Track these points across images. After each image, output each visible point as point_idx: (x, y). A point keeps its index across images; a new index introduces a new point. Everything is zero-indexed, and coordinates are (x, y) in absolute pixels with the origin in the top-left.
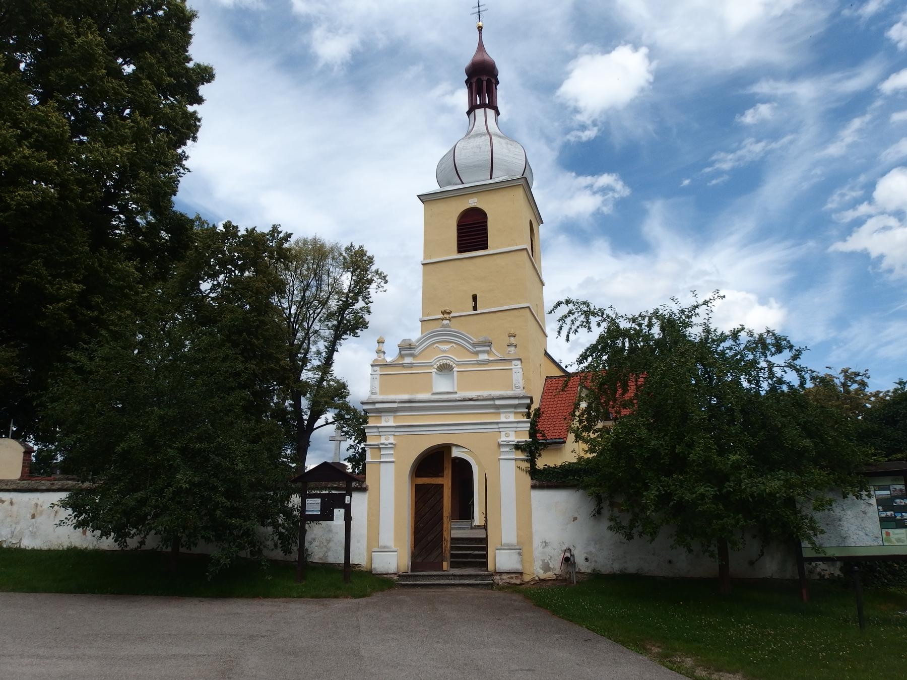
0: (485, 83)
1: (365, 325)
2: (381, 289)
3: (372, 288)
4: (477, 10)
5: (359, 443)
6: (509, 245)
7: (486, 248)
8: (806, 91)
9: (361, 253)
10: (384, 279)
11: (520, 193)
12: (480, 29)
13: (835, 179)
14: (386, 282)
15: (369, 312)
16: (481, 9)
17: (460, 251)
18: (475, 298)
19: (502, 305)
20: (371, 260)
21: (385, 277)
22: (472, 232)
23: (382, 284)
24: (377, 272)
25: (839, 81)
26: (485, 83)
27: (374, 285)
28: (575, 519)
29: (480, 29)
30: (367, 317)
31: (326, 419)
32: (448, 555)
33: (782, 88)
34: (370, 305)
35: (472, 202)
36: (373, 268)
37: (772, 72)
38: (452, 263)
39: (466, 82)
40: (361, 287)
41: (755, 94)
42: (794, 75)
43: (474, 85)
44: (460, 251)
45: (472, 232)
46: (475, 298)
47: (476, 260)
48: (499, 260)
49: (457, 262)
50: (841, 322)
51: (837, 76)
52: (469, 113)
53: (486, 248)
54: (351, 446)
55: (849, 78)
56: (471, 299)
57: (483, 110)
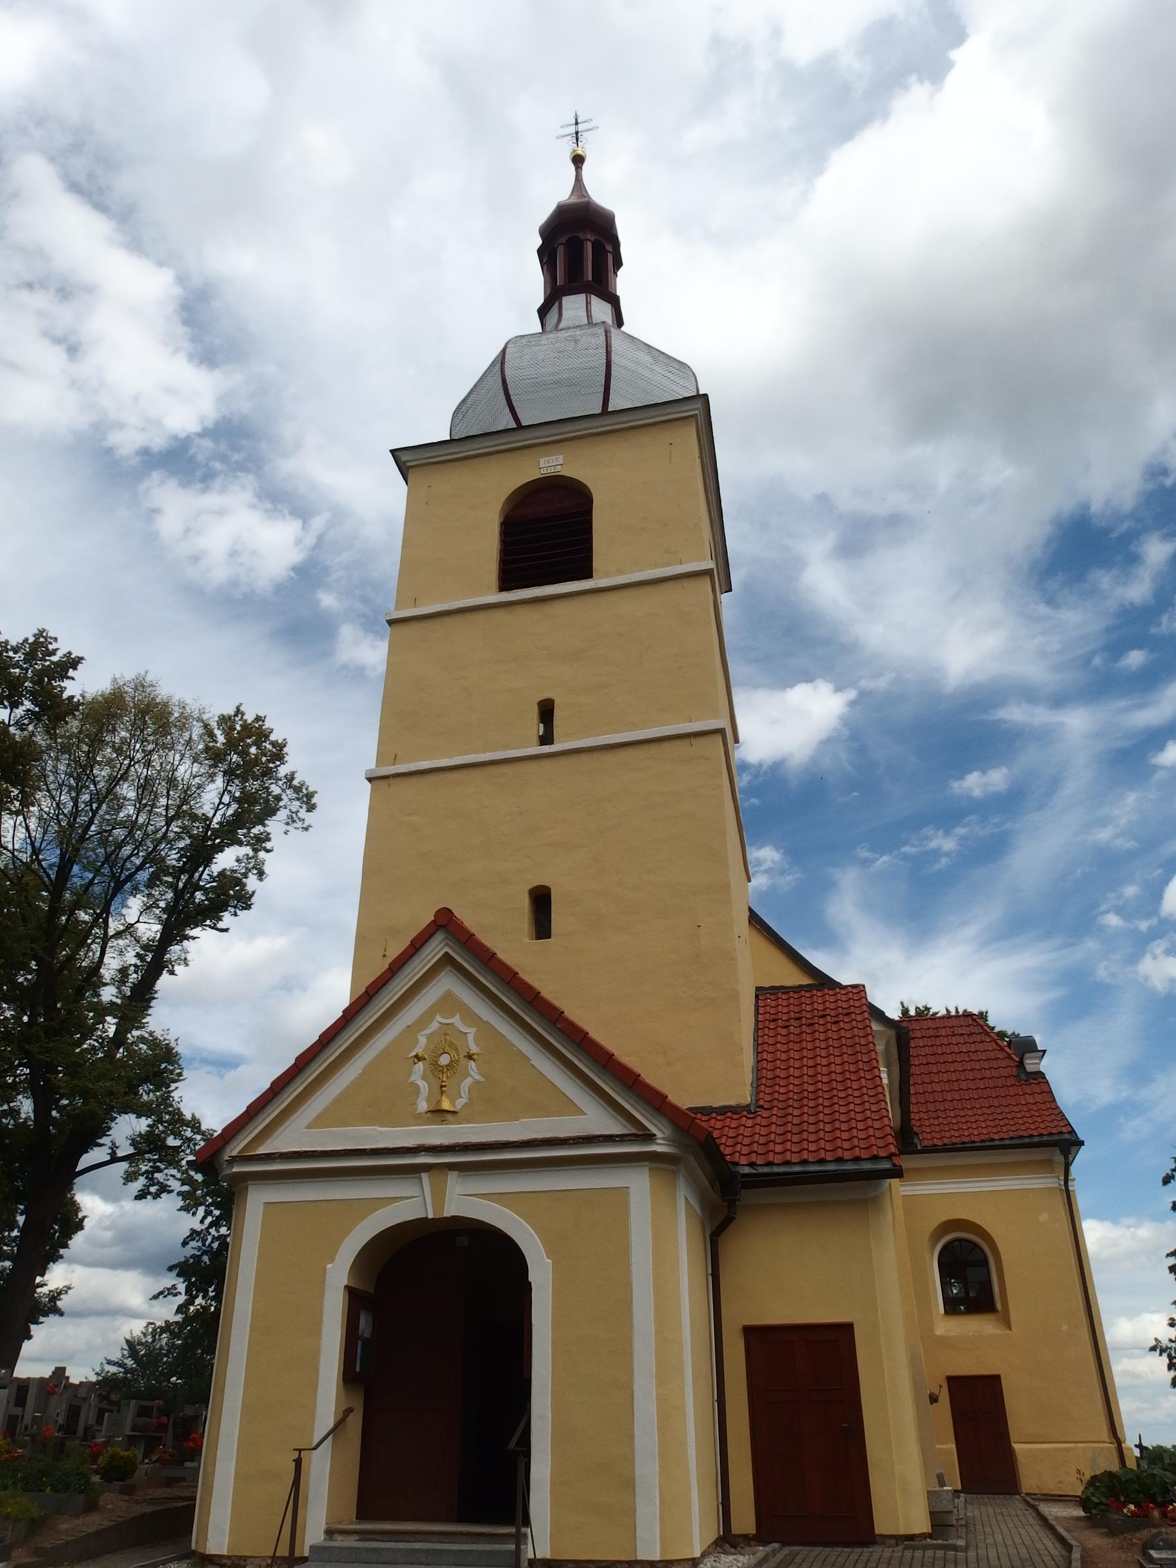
0: (589, 247)
1: (244, 901)
2: (299, 824)
3: (274, 826)
4: (573, 129)
5: (215, 1224)
6: (656, 566)
7: (588, 575)
8: (1077, 722)
9: (257, 732)
10: (308, 800)
11: (688, 436)
12: (578, 160)
13: (1107, 867)
14: (311, 808)
15: (261, 874)
16: (581, 127)
17: (505, 584)
18: (546, 711)
19: (633, 726)
20: (278, 754)
21: (310, 796)
22: (547, 539)
23: (303, 813)
24: (290, 778)
25: (1126, 710)
26: (589, 247)
27: (282, 815)
28: (934, 1399)
29: (578, 160)
30: (252, 883)
31: (114, 1147)
32: (880, 1059)
33: (1041, 716)
34: (262, 855)
35: (551, 464)
36: (283, 771)
37: (1027, 693)
38: (481, 616)
39: (540, 252)
40: (250, 814)
41: (1003, 721)
42: (1059, 701)
43: (561, 251)
44: (505, 584)
45: (547, 539)
46: (546, 711)
47: (556, 619)
48: (625, 604)
49: (499, 616)
50: (1137, 1074)
51: (1122, 703)
52: (543, 312)
53: (586, 572)
54: (194, 1234)
55: (1140, 707)
56: (535, 714)
57: (582, 297)
